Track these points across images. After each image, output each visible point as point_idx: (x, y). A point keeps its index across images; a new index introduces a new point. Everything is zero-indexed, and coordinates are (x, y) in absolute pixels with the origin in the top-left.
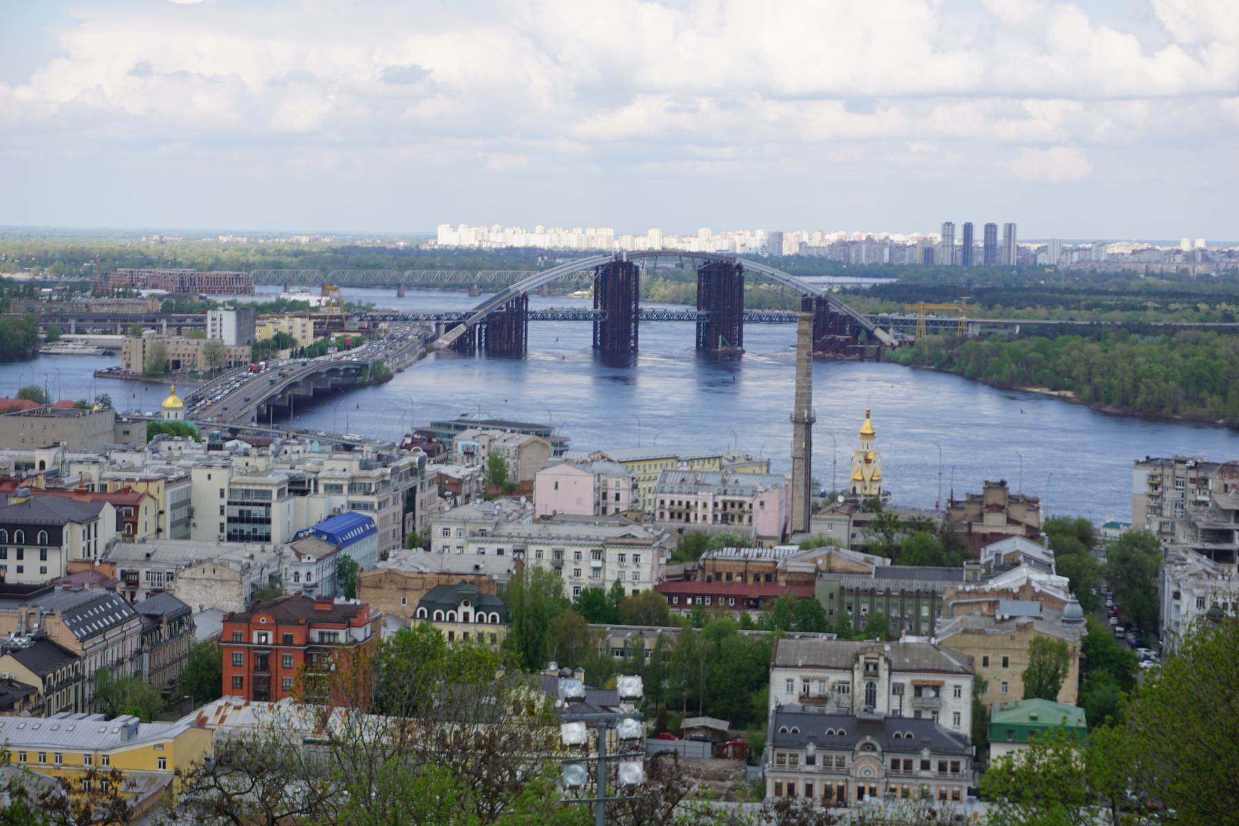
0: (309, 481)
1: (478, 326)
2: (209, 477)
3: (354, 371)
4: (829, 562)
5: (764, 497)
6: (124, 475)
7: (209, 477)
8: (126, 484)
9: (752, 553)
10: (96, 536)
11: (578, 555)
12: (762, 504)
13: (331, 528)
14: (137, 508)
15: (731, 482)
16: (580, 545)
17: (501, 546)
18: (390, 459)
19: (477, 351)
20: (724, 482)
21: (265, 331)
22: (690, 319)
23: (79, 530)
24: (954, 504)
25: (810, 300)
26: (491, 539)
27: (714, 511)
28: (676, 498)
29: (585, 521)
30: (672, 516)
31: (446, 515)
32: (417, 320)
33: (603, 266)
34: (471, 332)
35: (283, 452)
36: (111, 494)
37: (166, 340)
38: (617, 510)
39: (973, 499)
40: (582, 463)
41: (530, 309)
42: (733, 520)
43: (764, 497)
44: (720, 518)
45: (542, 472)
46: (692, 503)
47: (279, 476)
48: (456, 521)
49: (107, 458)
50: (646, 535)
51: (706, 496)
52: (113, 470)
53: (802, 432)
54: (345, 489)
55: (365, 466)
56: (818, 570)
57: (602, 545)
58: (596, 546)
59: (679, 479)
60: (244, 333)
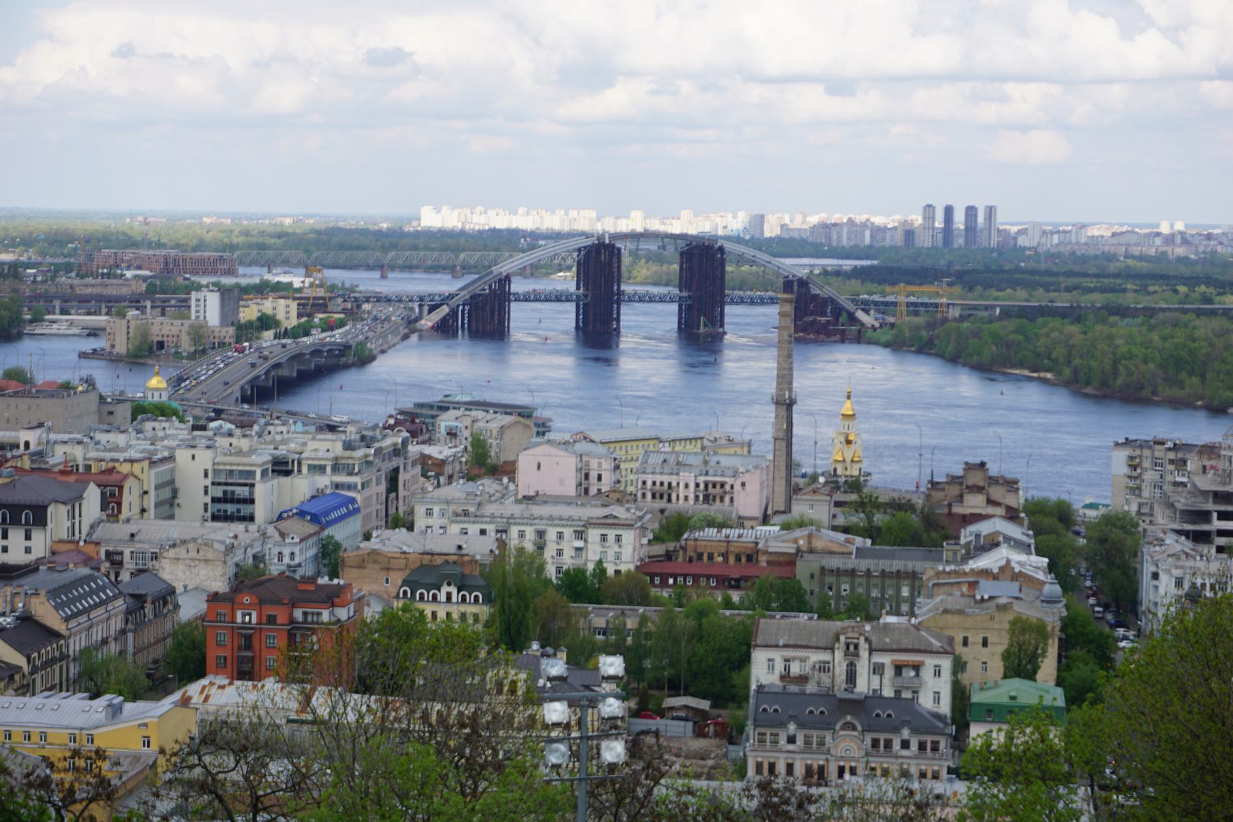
0: (293, 461)
1: (461, 308)
2: (193, 457)
3: (337, 352)
4: (810, 543)
5: (746, 478)
6: (108, 455)
7: (193, 457)
8: (111, 465)
9: (733, 533)
10: (80, 516)
11: (560, 536)
12: (743, 484)
13: (315, 508)
14: (121, 488)
15: (713, 463)
16: (563, 526)
17: (484, 527)
19: (460, 332)
20: (706, 463)
21: (249, 313)
22: (672, 301)
23: (63, 510)
24: (934, 485)
25: (792, 282)
26: (473, 519)
27: (695, 491)
28: (658, 478)
29: (567, 501)
30: (654, 496)
31: (429, 495)
32: (400, 301)
33: (585, 247)
34: (453, 313)
35: (266, 432)
36: (95, 474)
37: (150, 321)
39: (954, 480)
41: (512, 290)
42: (714, 500)
43: (746, 478)
44: (701, 498)
45: (525, 453)
46: (674, 484)
47: (263, 457)
48: (439, 501)
49: (91, 438)
50: (628, 515)
51: (687, 477)
52: (98, 450)
53: (783, 412)
54: (329, 469)
55: (348, 446)
56: (799, 550)
58: (579, 526)
60: (228, 314)
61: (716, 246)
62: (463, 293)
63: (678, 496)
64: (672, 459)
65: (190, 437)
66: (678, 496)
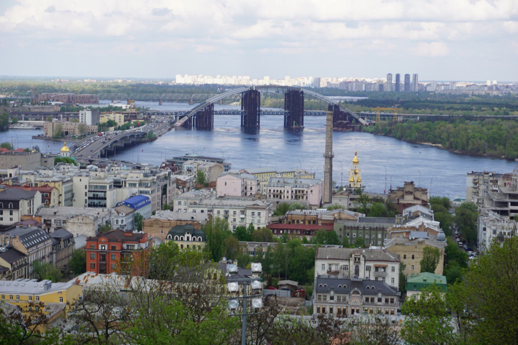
0: (122, 182)
1: (193, 117)
2: (81, 180)
3: (141, 136)
4: (339, 216)
5: (313, 189)
6: (45, 179)
7: (81, 180)
8: (46, 183)
9: (307, 212)
10: (33, 205)
11: (235, 213)
12: (312, 191)
13: (132, 201)
14: (50, 193)
16: (236, 209)
17: (202, 209)
18: (156, 173)
20: (296, 182)
21: (104, 119)
23: (26, 202)
24: (392, 191)
28: (276, 189)
29: (238, 198)
30: (274, 196)
31: (180, 196)
32: (167, 114)
34: (190, 120)
35: (111, 170)
36: (39, 187)
37: (62, 123)
38: (251, 194)
39: (400, 189)
40: (236, 174)
42: (299, 198)
43: (313, 189)
44: (294, 197)
45: (220, 178)
46: (283, 191)
47: (110, 180)
48: (184, 198)
49: (38, 172)
50: (263, 204)
51: (288, 188)
52: (40, 177)
53: (328, 161)
54: (137, 185)
55: (146, 175)
56: (335, 219)
57: (245, 209)
58: (242, 209)
59: (277, 181)
60: (95, 120)
61: (300, 91)
62: (194, 111)
63: (284, 196)
64: (282, 181)
65: (79, 172)
66: (284, 196)
